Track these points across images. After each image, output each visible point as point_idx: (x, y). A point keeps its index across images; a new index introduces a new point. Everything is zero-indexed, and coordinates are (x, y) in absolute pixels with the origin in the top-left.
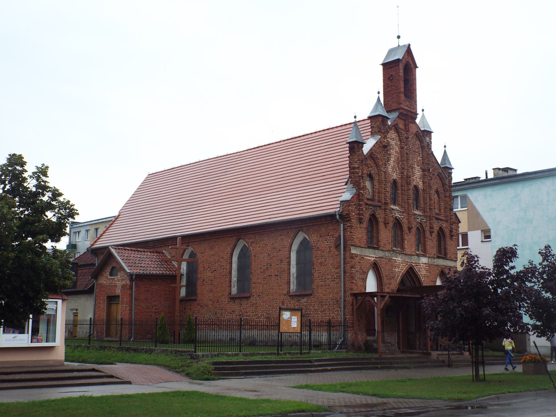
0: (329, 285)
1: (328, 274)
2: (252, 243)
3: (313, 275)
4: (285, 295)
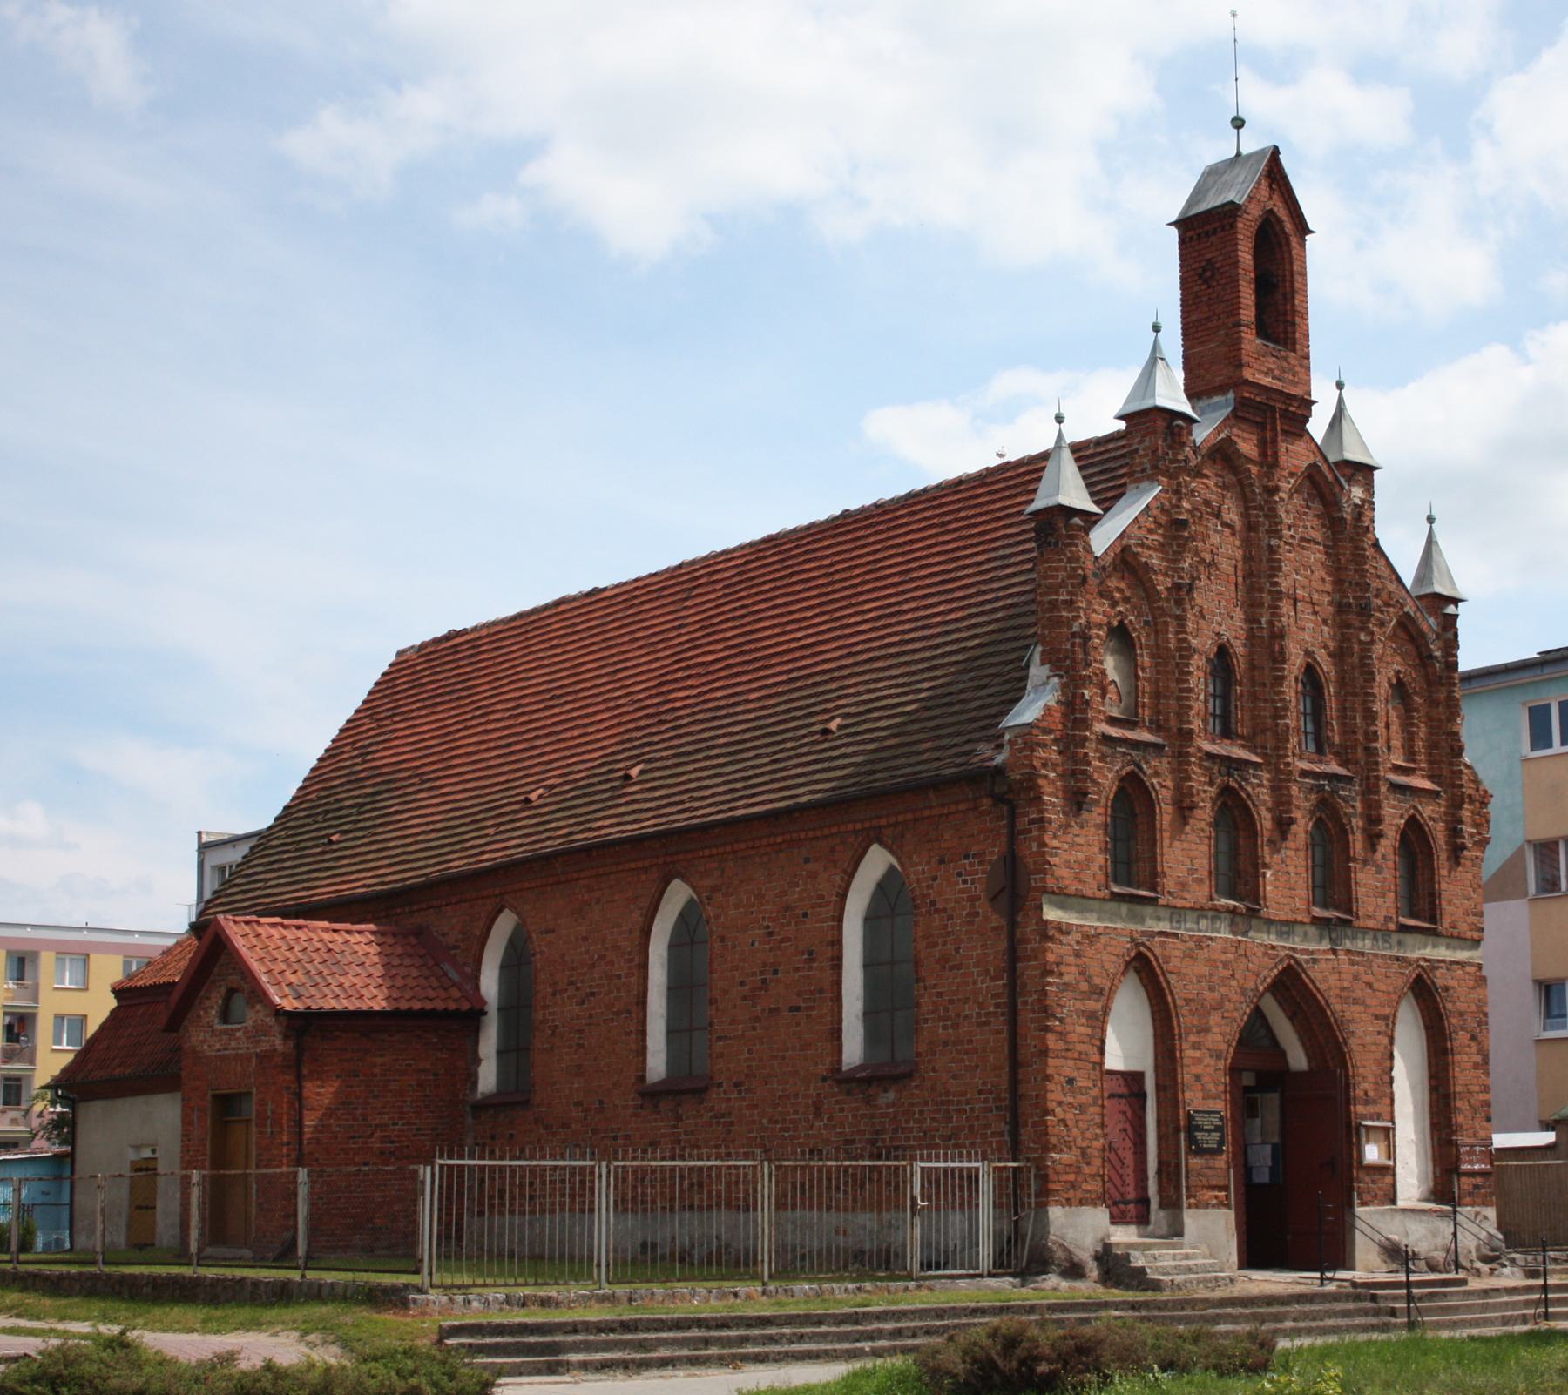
0: (970, 1041)
1: (967, 1000)
2: (715, 889)
3: (918, 1005)
4: (824, 1079)
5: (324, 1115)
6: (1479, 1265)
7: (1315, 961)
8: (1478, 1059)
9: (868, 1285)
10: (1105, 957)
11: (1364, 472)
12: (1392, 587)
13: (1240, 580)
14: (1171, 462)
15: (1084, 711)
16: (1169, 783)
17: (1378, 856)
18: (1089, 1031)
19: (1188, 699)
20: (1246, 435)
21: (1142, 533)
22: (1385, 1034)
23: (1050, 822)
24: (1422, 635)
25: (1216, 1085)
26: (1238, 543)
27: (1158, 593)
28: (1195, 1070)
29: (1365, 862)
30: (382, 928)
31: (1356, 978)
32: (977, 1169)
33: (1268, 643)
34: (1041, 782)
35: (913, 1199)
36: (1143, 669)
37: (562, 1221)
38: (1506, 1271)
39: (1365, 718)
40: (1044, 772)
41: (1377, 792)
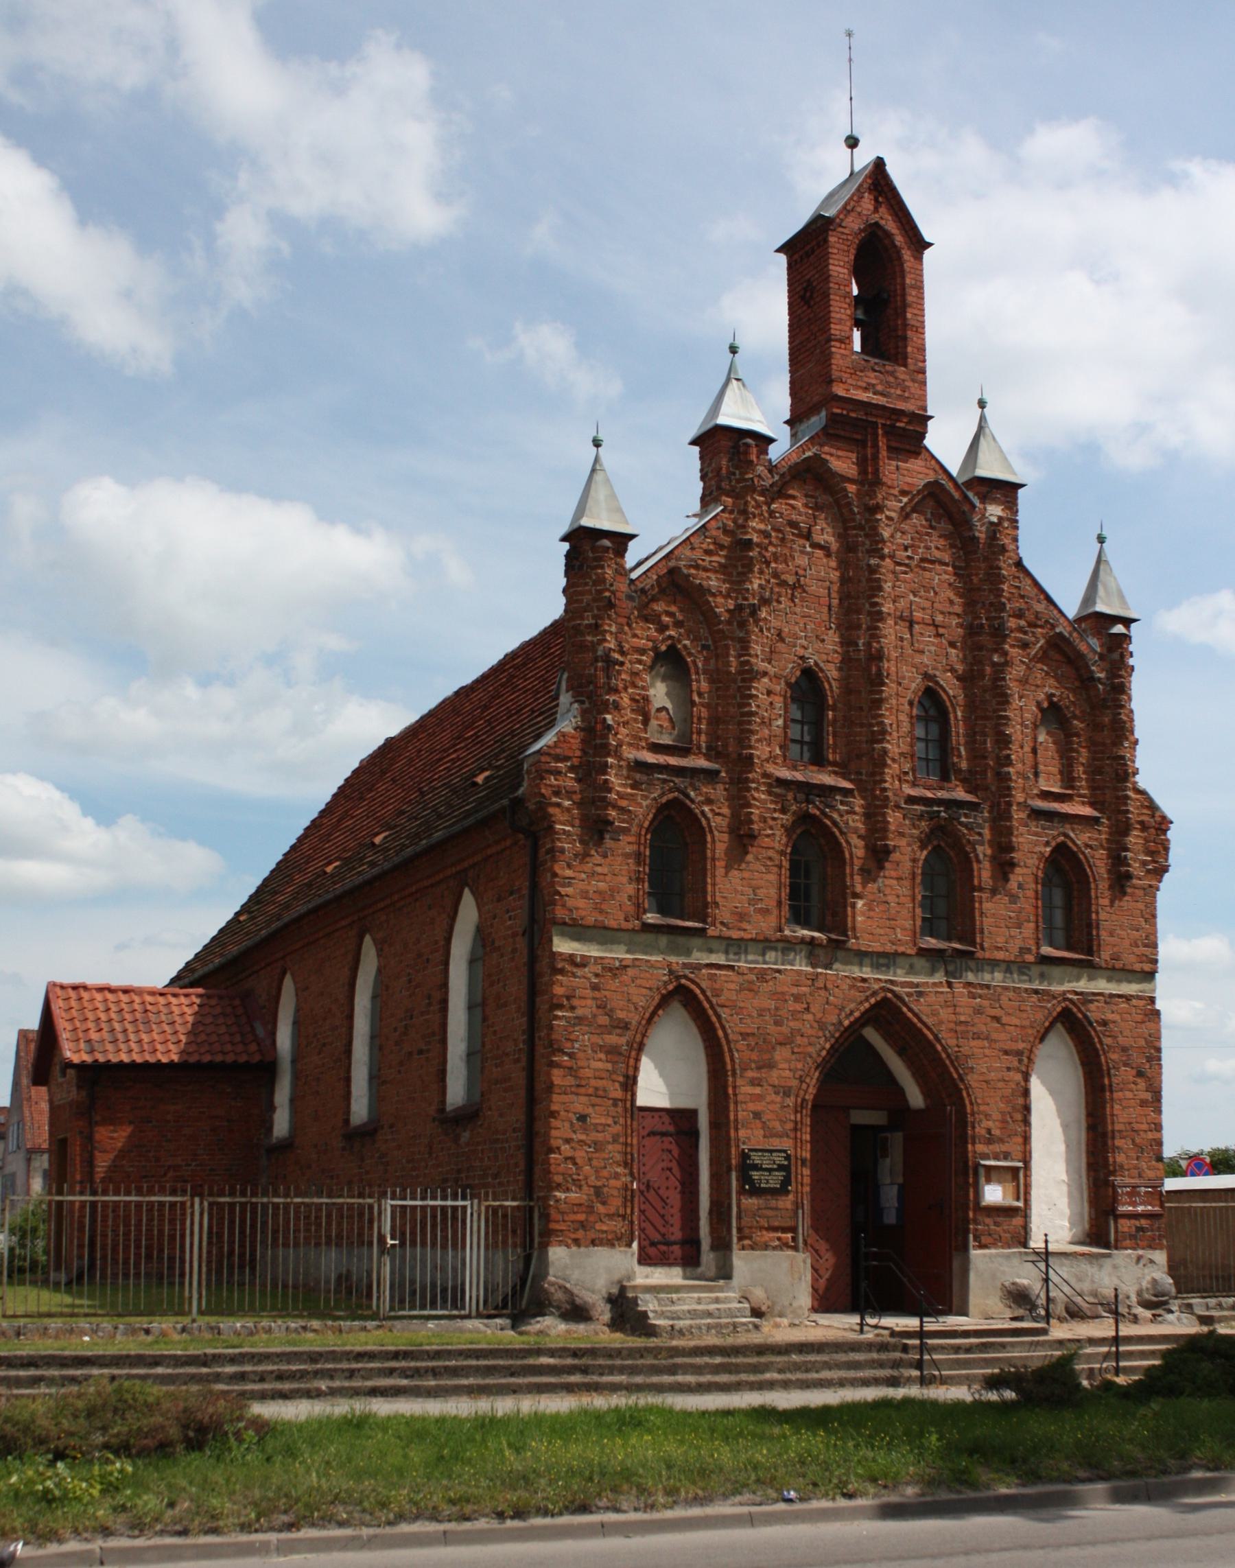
5: (116, 1157)
6: (1139, 1311)
7: (920, 994)
8: (1148, 1096)
9: (315, 1324)
10: (633, 990)
11: (1007, 491)
12: (1040, 607)
13: (835, 602)
14: (738, 481)
15: (606, 737)
16: (726, 811)
17: (1013, 885)
18: (609, 1066)
19: (749, 723)
20: (840, 453)
21: (698, 554)
22: (1018, 1070)
23: (562, 851)
24: (1081, 656)
25: (782, 1122)
26: (833, 564)
27: (717, 616)
28: (752, 1107)
29: (994, 892)
30: (210, 992)
31: (978, 1011)
32: (464, 1208)
33: (864, 669)
34: (551, 810)
35: (382, 1239)
36: (700, 695)
37: (423, 1256)
38: (1170, 1317)
39: (997, 742)
40: (554, 800)
41: (1010, 818)
